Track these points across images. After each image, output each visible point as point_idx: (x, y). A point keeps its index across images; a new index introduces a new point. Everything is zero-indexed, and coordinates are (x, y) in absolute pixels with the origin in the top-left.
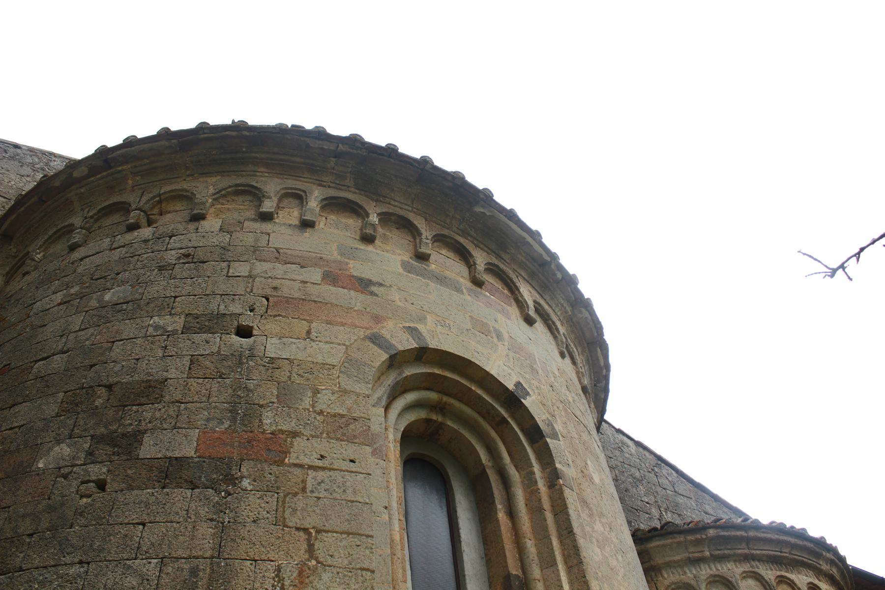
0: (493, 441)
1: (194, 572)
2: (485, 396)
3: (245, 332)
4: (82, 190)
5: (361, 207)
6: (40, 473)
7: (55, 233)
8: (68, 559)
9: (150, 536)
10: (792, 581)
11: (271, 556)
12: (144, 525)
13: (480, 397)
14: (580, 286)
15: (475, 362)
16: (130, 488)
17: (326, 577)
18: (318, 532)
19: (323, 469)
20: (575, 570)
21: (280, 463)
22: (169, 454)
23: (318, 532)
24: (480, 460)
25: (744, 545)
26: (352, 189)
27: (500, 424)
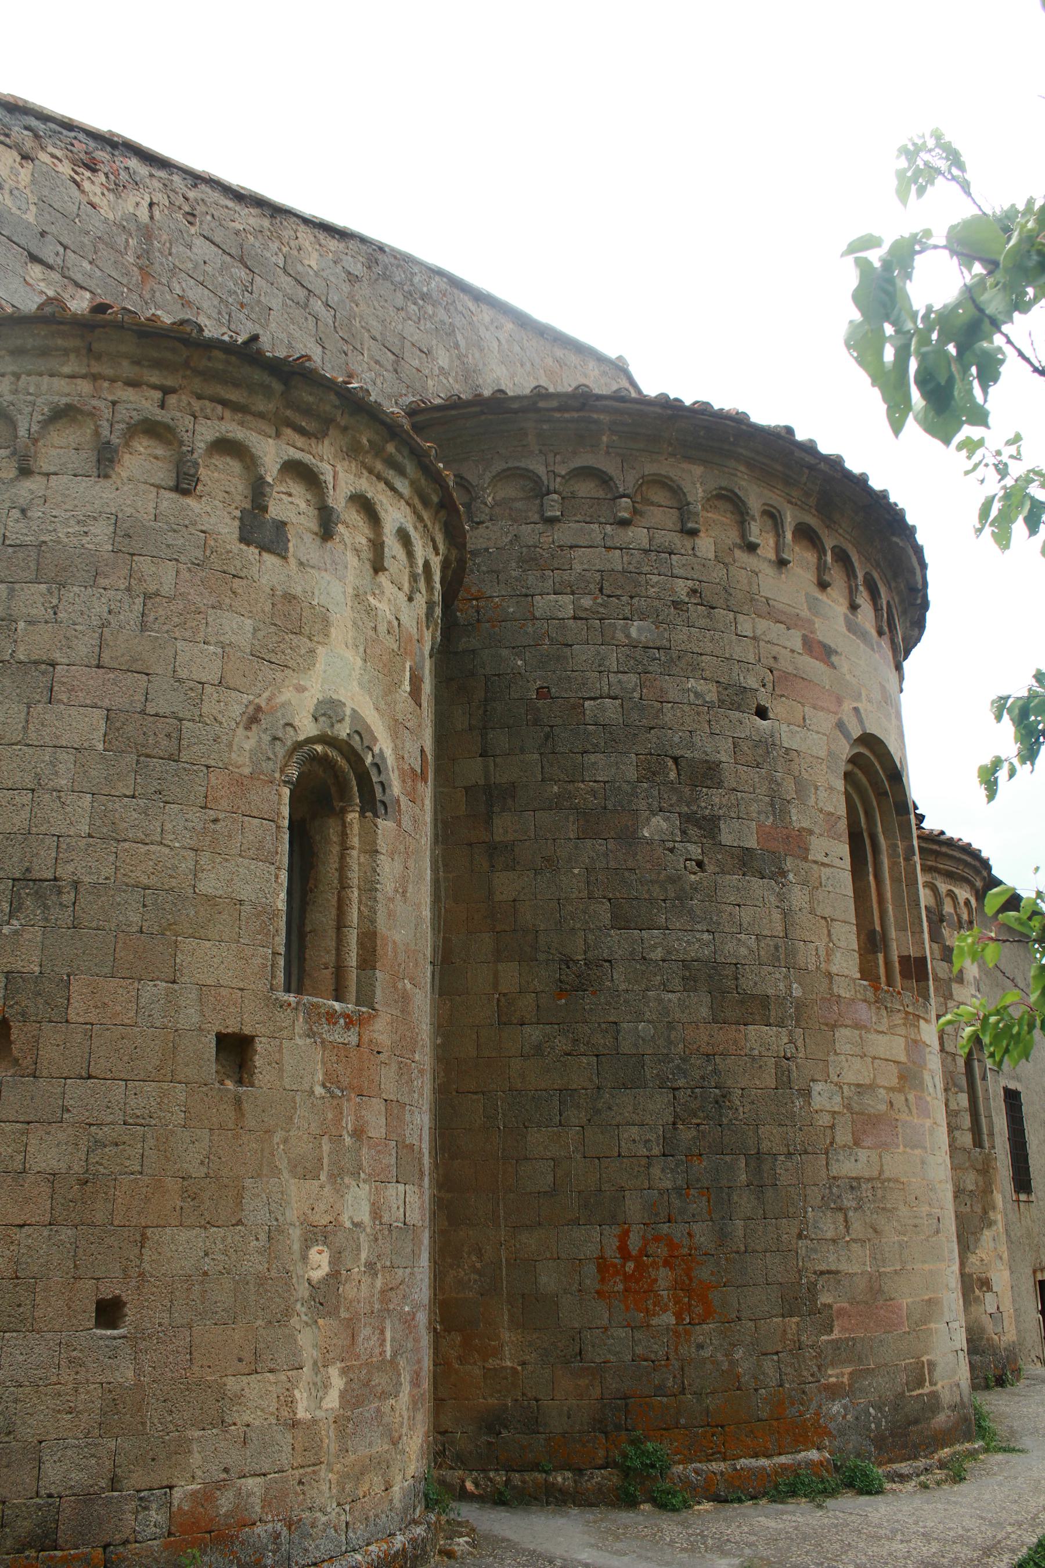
0: (873, 808)
1: (777, 948)
2: (876, 764)
3: (762, 713)
4: (545, 427)
5: (819, 539)
6: (650, 842)
7: (504, 471)
8: (698, 927)
9: (746, 915)
10: (956, 895)
11: (813, 938)
12: (739, 906)
13: (877, 772)
14: (928, 614)
15: (599, 466)
16: (723, 872)
17: (838, 955)
18: (832, 920)
19: (828, 865)
20: (917, 936)
21: (805, 859)
22: (742, 844)
23: (832, 920)
24: (860, 822)
25: (933, 858)
26: (813, 511)
27: (881, 794)
